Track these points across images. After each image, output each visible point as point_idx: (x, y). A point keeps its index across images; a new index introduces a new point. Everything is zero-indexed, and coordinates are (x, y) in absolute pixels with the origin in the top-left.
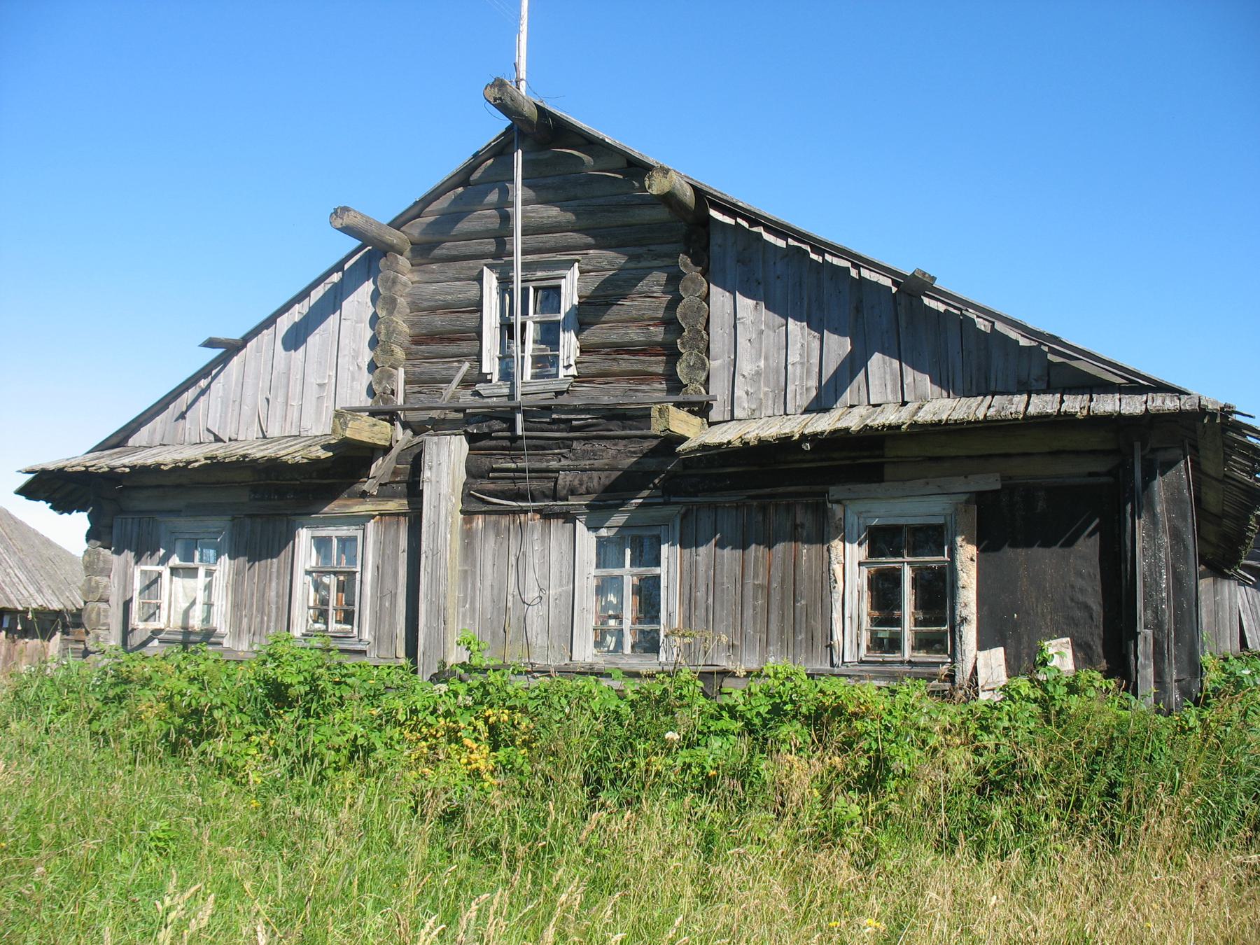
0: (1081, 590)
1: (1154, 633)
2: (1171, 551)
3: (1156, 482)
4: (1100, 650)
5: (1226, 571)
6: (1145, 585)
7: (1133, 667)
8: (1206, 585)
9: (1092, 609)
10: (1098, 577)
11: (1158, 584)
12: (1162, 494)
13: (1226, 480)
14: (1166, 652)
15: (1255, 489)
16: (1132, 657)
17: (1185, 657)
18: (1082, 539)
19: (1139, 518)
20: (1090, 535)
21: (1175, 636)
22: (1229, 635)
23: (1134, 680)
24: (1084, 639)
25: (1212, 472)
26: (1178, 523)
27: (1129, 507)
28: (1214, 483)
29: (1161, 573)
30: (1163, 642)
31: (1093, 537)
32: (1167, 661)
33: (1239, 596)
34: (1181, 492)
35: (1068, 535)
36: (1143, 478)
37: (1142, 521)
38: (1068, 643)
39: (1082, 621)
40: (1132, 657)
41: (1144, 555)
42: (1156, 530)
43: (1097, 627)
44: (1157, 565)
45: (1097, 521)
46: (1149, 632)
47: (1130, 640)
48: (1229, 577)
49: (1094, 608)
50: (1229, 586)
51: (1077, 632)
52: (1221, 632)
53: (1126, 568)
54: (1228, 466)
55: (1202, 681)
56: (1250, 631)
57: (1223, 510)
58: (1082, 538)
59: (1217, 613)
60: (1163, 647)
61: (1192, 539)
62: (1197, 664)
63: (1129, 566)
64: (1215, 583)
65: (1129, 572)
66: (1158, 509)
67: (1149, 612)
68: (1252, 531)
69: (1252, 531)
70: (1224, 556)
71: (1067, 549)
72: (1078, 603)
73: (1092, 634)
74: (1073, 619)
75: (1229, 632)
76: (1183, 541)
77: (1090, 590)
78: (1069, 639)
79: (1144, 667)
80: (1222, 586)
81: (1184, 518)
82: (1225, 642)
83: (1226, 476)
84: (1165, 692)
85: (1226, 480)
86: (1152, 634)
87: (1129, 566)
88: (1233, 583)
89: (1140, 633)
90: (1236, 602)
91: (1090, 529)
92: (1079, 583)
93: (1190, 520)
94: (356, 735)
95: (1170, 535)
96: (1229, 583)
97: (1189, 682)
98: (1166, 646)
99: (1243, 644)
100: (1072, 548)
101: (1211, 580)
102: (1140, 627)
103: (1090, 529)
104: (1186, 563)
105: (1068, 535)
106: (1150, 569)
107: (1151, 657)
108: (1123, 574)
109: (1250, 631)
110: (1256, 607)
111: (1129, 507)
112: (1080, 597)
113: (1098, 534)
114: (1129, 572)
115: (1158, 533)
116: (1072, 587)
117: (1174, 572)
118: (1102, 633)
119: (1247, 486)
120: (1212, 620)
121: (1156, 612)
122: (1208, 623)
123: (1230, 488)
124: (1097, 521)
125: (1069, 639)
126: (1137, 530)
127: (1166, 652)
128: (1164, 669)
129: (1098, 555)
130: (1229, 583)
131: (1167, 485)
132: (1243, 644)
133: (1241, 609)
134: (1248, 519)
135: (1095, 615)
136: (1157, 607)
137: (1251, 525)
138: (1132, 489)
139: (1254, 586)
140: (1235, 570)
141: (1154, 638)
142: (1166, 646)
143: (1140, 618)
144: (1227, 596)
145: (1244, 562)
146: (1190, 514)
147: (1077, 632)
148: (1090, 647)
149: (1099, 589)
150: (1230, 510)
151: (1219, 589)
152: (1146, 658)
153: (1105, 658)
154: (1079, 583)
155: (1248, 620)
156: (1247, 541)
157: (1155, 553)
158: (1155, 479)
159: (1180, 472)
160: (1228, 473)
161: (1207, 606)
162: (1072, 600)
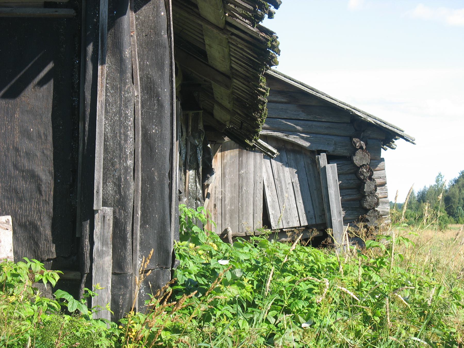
0: (28, 154)
1: (114, 212)
2: (142, 107)
3: (125, 18)
4: (48, 232)
5: (247, 141)
6: (106, 150)
7: (87, 255)
8: (231, 157)
9: (41, 180)
10: (50, 138)
11: (121, 149)
12: (134, 34)
13: (229, 28)
14: (129, 235)
15: (258, 40)
16: (87, 242)
17: (153, 242)
18: (30, 87)
19: (103, 63)
20: (41, 83)
21: (142, 215)
22: (251, 211)
23: (87, 271)
24: (29, 218)
25: (211, 17)
26: (154, 73)
27: (90, 48)
28: (215, 31)
29: (126, 136)
30: (126, 223)
31: (45, 87)
32: (129, 247)
33: (264, 170)
34: (157, 34)
35: (13, 82)
36: (110, 11)
37: (106, 67)
38: (7, 222)
39: (27, 195)
40: (87, 242)
41: (107, 112)
42: (122, 80)
43: (46, 202)
44: (122, 125)
45: (50, 66)
46: (109, 211)
47: (85, 220)
48: (252, 149)
49: (43, 177)
50: (255, 159)
51: (21, 208)
52: (244, 209)
53: (84, 127)
54: (230, 10)
55: (172, 272)
56: (274, 208)
57: (231, 67)
58: (31, 86)
59: (240, 188)
60: (125, 230)
61: (168, 94)
62: (167, 252)
63: (87, 125)
64: (240, 155)
65: (87, 133)
66: (127, 53)
67: (110, 187)
68: (263, 94)
69: (263, 94)
70: (242, 123)
71: (12, 101)
72: (23, 171)
73: (39, 211)
74: (17, 193)
75: (252, 208)
76: (158, 96)
77: (38, 154)
78: (9, 218)
79: (101, 254)
80: (247, 159)
81: (161, 67)
82: (247, 219)
83: (227, 23)
84: (126, 287)
85: (229, 28)
86: (111, 213)
87: (87, 125)
88: (259, 156)
89: (97, 211)
90: (261, 176)
91: (42, 74)
92: (26, 145)
93: (167, 70)
94: (368, 221)
95: (142, 88)
96: (255, 156)
97: (157, 275)
98: (129, 228)
99: (266, 222)
100: (18, 99)
101: (236, 152)
102: (97, 204)
103: (42, 74)
104: (160, 123)
105: (13, 82)
106: (113, 131)
107: (110, 241)
108: (81, 135)
109: (274, 208)
110: (281, 182)
111: (90, 48)
112: (25, 163)
113: (52, 82)
114: (87, 133)
115: (125, 84)
116: (17, 150)
117: (145, 135)
118: (52, 210)
119: (251, 36)
120: (236, 195)
121: (118, 185)
122: (232, 199)
123: (234, 40)
124: (50, 66)
125: (9, 218)
126: (99, 79)
127: (129, 235)
128: (125, 258)
129: (51, 110)
130: (255, 156)
131: (141, 24)
132: (266, 222)
133: (266, 184)
134: (257, 80)
135: (44, 188)
136: (119, 179)
137: (261, 87)
138: (96, 26)
139: (279, 159)
140: (255, 140)
141: (115, 217)
142: (129, 228)
143: (98, 192)
144: (252, 169)
145: (262, 132)
146: (167, 62)
147: (21, 208)
148: (36, 228)
149: (50, 153)
150: (239, 69)
151: (244, 161)
152: (104, 243)
153: (53, 243)
154: (26, 145)
155: (272, 195)
156: (260, 107)
157: (120, 110)
158: (124, 14)
159: (158, 7)
160: (230, 20)
161: (231, 180)
162: (16, 167)
